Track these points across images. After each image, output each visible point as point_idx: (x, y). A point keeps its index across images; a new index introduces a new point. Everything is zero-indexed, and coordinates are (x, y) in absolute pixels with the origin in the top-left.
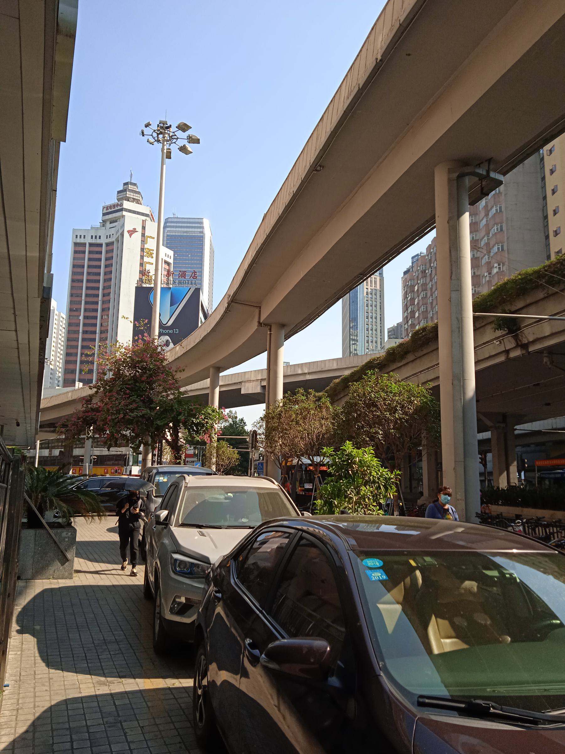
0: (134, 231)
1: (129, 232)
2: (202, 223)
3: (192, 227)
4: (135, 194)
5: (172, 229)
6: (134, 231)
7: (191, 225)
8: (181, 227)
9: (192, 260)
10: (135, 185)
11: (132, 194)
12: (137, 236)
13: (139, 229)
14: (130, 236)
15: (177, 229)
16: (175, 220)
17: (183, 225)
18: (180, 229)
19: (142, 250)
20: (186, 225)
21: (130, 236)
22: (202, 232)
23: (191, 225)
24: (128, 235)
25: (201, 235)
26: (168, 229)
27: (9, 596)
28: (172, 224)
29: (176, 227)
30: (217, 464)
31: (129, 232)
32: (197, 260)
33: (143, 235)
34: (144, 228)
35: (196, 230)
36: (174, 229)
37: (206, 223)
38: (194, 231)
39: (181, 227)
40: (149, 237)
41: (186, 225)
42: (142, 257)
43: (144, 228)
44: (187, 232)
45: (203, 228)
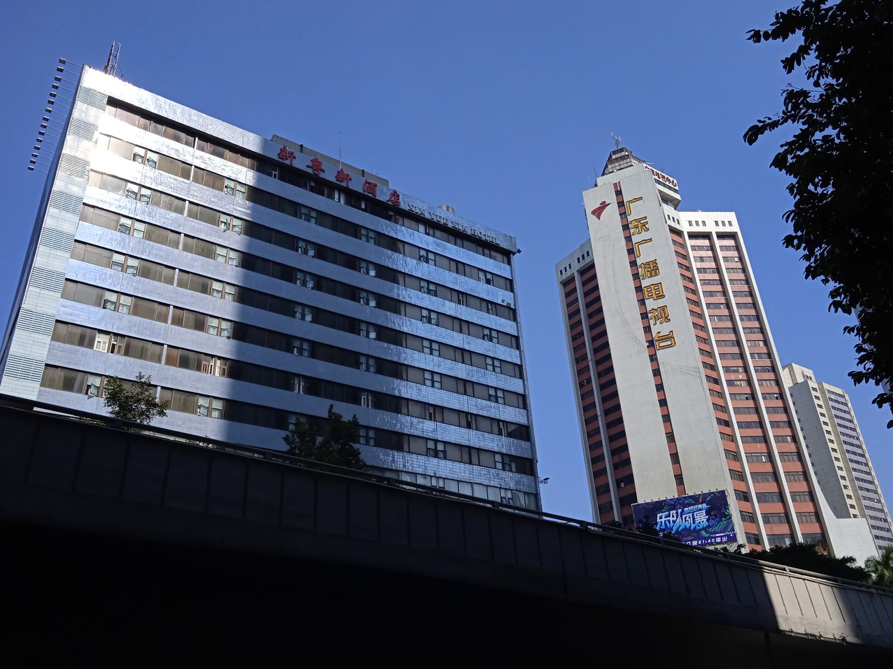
0: (604, 205)
1: (594, 212)
4: (622, 162)
6: (604, 205)
11: (617, 164)
12: (612, 211)
13: (612, 199)
14: (599, 217)
19: (626, 227)
21: (599, 217)
24: (595, 217)
31: (594, 212)
33: (621, 204)
34: (619, 193)
42: (628, 239)
43: (619, 193)
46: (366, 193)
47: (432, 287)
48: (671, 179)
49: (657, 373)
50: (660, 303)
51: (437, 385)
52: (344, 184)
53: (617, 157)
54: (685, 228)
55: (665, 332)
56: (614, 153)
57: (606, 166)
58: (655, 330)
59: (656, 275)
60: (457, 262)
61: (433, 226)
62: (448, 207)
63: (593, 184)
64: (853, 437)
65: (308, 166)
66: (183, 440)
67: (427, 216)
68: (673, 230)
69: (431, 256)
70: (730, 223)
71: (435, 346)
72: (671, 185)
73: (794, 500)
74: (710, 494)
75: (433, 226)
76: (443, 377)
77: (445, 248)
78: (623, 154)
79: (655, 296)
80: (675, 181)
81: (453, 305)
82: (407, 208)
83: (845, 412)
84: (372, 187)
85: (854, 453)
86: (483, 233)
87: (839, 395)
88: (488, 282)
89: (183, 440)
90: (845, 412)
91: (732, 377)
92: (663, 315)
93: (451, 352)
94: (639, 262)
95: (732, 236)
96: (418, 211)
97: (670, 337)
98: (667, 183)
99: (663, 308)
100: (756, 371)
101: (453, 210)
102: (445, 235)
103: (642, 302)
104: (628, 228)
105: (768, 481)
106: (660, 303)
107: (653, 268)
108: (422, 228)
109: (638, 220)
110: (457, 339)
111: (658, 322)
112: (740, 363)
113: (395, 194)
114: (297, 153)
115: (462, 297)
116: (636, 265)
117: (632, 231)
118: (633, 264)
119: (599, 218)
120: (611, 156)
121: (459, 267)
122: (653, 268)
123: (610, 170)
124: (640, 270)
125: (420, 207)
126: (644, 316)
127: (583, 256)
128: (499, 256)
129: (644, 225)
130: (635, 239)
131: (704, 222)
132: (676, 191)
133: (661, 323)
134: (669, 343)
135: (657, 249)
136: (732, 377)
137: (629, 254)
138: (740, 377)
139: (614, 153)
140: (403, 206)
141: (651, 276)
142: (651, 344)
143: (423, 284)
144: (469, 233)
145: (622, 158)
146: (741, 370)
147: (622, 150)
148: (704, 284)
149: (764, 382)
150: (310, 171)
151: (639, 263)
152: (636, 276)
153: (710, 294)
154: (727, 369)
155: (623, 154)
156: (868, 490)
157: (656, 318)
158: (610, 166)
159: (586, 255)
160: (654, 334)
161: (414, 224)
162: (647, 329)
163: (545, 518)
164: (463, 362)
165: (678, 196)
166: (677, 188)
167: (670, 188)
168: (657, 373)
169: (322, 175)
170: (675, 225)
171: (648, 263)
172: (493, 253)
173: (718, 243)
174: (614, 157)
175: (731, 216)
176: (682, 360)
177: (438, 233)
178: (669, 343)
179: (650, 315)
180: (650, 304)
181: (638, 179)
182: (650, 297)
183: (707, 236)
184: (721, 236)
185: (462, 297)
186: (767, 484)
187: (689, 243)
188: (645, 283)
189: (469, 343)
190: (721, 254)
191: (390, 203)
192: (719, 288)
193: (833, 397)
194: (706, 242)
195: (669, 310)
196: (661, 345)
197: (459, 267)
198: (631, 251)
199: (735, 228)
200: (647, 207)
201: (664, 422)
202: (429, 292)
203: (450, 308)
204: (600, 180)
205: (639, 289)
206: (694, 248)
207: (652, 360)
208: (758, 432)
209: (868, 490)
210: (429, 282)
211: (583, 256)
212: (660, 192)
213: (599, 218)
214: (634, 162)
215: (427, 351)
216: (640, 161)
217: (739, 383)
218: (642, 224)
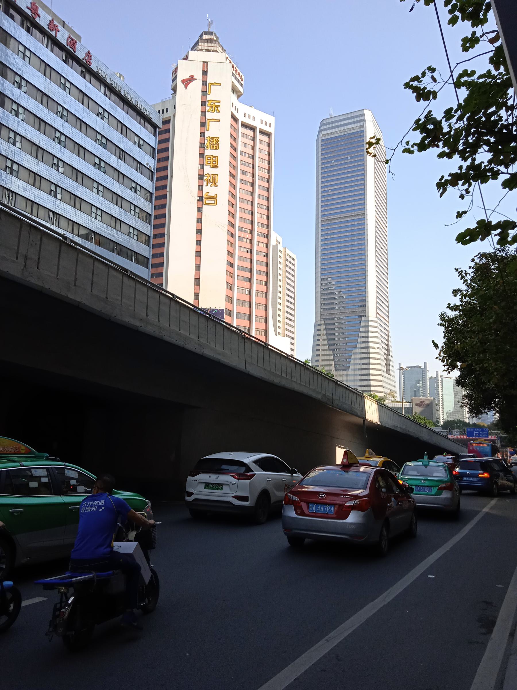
0: (192, 79)
1: (183, 81)
2: (363, 115)
3: (350, 123)
4: (210, 45)
5: (327, 132)
6: (192, 79)
7: (349, 121)
8: (338, 127)
9: (352, 162)
10: (212, 33)
11: (206, 44)
12: (196, 86)
13: (199, 76)
14: (186, 87)
15: (333, 130)
16: (331, 120)
17: (340, 123)
18: (336, 130)
19: (204, 103)
20: (343, 123)
21: (186, 87)
22: (363, 126)
23: (349, 121)
24: (183, 86)
25: (362, 129)
26: (323, 133)
27: (347, 491)
28: (327, 126)
29: (332, 128)
30: (153, 526)
31: (183, 81)
32: (358, 161)
33: (204, 83)
34: (205, 73)
35: (355, 125)
36: (330, 131)
37: (368, 115)
38: (354, 128)
39: (338, 127)
40: (212, 84)
41: (343, 123)
42: (204, 113)
43: (205, 73)
44: (344, 131)
45: (364, 120)
46: (68, 47)
47: (104, 141)
48: (241, 74)
49: (199, 221)
50: (213, 171)
51: (99, 218)
52: (53, 33)
53: (206, 39)
54: (241, 118)
55: (212, 194)
56: (206, 33)
57: (197, 43)
58: (206, 189)
59: (216, 149)
60: (123, 124)
61: (111, 90)
62: (120, 75)
63: (184, 56)
64: (292, 286)
65: (28, 8)
66: (191, 307)
67: (109, 81)
68: (233, 117)
69: (106, 115)
70: (270, 126)
71: (101, 188)
72: (239, 79)
73: (256, 321)
74: (214, 310)
75: (111, 90)
76: (103, 213)
77: (116, 111)
78: (212, 37)
79: (211, 165)
80: (243, 78)
81: (116, 159)
82: (95, 70)
83: (292, 270)
84: (73, 44)
85: (290, 296)
86: (143, 106)
87: (293, 259)
88: (140, 146)
89: (191, 307)
90: (292, 270)
91: (243, 235)
92: (214, 180)
93: (110, 195)
94: (207, 134)
95: (269, 135)
96: (103, 74)
97: (214, 198)
98: (238, 76)
99: (215, 176)
100: (258, 235)
101: (124, 78)
102: (117, 100)
103: (202, 166)
104: (205, 105)
105: (245, 306)
106: (213, 171)
107: (215, 143)
108: (103, 89)
109: (214, 102)
110: (115, 186)
111: (209, 185)
112: (249, 226)
113: (88, 54)
114: (60, 27)
115: (122, 154)
116: (204, 136)
117: (208, 108)
118: (202, 135)
119: (186, 88)
120: (202, 35)
121: (124, 129)
122: (215, 143)
123: (200, 47)
124: (206, 141)
125: (104, 72)
126: (201, 177)
127: (163, 111)
128: (149, 127)
129: (217, 107)
130: (209, 115)
131: (254, 118)
132: (241, 85)
133: (211, 186)
134: (213, 202)
135: (220, 129)
136: (243, 235)
137: (201, 126)
138: (247, 236)
139: (206, 33)
140: (94, 67)
141: (213, 149)
142: (200, 199)
143: (99, 137)
144: (134, 103)
145: (211, 41)
146: (249, 231)
147: (212, 33)
148: (242, 164)
149: (260, 243)
150: (29, 12)
151: (206, 136)
152: (202, 145)
153: (244, 173)
154: (241, 229)
155: (212, 37)
156: (290, 320)
157: (208, 182)
158: (200, 44)
159: (165, 111)
160: (205, 192)
161: (97, 83)
162: (201, 188)
163: (269, 347)
164: (76, 181)
165: (241, 90)
166: (243, 83)
167: (238, 81)
168: (199, 221)
169: (37, 19)
170: (235, 113)
171: (213, 138)
172: (147, 124)
173: (259, 136)
174: (204, 36)
175: (271, 119)
176: (216, 217)
177: (113, 96)
178: (213, 202)
179: (205, 178)
180: (207, 170)
181: (220, 66)
182: (208, 164)
183: (253, 129)
184: (262, 132)
185: (122, 154)
186: (244, 308)
187: (241, 130)
188: (207, 152)
189: (122, 191)
190: (258, 146)
191: (84, 61)
192: (250, 170)
193: (289, 259)
194: (251, 133)
195: (219, 179)
196: (207, 202)
197: (124, 129)
198: (203, 124)
199: (271, 130)
200: (222, 94)
201: (196, 256)
202: (101, 144)
203: (114, 161)
204: (192, 55)
205: (202, 155)
206: (243, 134)
207: (198, 211)
208: (248, 275)
209: (290, 320)
210: (102, 136)
211: (163, 111)
212: (232, 82)
213: (186, 88)
214: (219, 49)
215: (95, 190)
216: (225, 51)
217: (245, 240)
218: (216, 106)
